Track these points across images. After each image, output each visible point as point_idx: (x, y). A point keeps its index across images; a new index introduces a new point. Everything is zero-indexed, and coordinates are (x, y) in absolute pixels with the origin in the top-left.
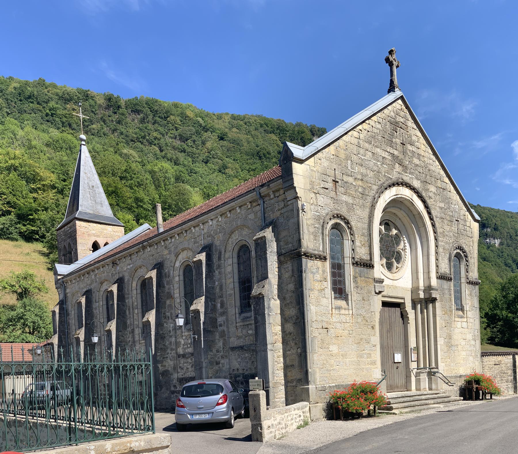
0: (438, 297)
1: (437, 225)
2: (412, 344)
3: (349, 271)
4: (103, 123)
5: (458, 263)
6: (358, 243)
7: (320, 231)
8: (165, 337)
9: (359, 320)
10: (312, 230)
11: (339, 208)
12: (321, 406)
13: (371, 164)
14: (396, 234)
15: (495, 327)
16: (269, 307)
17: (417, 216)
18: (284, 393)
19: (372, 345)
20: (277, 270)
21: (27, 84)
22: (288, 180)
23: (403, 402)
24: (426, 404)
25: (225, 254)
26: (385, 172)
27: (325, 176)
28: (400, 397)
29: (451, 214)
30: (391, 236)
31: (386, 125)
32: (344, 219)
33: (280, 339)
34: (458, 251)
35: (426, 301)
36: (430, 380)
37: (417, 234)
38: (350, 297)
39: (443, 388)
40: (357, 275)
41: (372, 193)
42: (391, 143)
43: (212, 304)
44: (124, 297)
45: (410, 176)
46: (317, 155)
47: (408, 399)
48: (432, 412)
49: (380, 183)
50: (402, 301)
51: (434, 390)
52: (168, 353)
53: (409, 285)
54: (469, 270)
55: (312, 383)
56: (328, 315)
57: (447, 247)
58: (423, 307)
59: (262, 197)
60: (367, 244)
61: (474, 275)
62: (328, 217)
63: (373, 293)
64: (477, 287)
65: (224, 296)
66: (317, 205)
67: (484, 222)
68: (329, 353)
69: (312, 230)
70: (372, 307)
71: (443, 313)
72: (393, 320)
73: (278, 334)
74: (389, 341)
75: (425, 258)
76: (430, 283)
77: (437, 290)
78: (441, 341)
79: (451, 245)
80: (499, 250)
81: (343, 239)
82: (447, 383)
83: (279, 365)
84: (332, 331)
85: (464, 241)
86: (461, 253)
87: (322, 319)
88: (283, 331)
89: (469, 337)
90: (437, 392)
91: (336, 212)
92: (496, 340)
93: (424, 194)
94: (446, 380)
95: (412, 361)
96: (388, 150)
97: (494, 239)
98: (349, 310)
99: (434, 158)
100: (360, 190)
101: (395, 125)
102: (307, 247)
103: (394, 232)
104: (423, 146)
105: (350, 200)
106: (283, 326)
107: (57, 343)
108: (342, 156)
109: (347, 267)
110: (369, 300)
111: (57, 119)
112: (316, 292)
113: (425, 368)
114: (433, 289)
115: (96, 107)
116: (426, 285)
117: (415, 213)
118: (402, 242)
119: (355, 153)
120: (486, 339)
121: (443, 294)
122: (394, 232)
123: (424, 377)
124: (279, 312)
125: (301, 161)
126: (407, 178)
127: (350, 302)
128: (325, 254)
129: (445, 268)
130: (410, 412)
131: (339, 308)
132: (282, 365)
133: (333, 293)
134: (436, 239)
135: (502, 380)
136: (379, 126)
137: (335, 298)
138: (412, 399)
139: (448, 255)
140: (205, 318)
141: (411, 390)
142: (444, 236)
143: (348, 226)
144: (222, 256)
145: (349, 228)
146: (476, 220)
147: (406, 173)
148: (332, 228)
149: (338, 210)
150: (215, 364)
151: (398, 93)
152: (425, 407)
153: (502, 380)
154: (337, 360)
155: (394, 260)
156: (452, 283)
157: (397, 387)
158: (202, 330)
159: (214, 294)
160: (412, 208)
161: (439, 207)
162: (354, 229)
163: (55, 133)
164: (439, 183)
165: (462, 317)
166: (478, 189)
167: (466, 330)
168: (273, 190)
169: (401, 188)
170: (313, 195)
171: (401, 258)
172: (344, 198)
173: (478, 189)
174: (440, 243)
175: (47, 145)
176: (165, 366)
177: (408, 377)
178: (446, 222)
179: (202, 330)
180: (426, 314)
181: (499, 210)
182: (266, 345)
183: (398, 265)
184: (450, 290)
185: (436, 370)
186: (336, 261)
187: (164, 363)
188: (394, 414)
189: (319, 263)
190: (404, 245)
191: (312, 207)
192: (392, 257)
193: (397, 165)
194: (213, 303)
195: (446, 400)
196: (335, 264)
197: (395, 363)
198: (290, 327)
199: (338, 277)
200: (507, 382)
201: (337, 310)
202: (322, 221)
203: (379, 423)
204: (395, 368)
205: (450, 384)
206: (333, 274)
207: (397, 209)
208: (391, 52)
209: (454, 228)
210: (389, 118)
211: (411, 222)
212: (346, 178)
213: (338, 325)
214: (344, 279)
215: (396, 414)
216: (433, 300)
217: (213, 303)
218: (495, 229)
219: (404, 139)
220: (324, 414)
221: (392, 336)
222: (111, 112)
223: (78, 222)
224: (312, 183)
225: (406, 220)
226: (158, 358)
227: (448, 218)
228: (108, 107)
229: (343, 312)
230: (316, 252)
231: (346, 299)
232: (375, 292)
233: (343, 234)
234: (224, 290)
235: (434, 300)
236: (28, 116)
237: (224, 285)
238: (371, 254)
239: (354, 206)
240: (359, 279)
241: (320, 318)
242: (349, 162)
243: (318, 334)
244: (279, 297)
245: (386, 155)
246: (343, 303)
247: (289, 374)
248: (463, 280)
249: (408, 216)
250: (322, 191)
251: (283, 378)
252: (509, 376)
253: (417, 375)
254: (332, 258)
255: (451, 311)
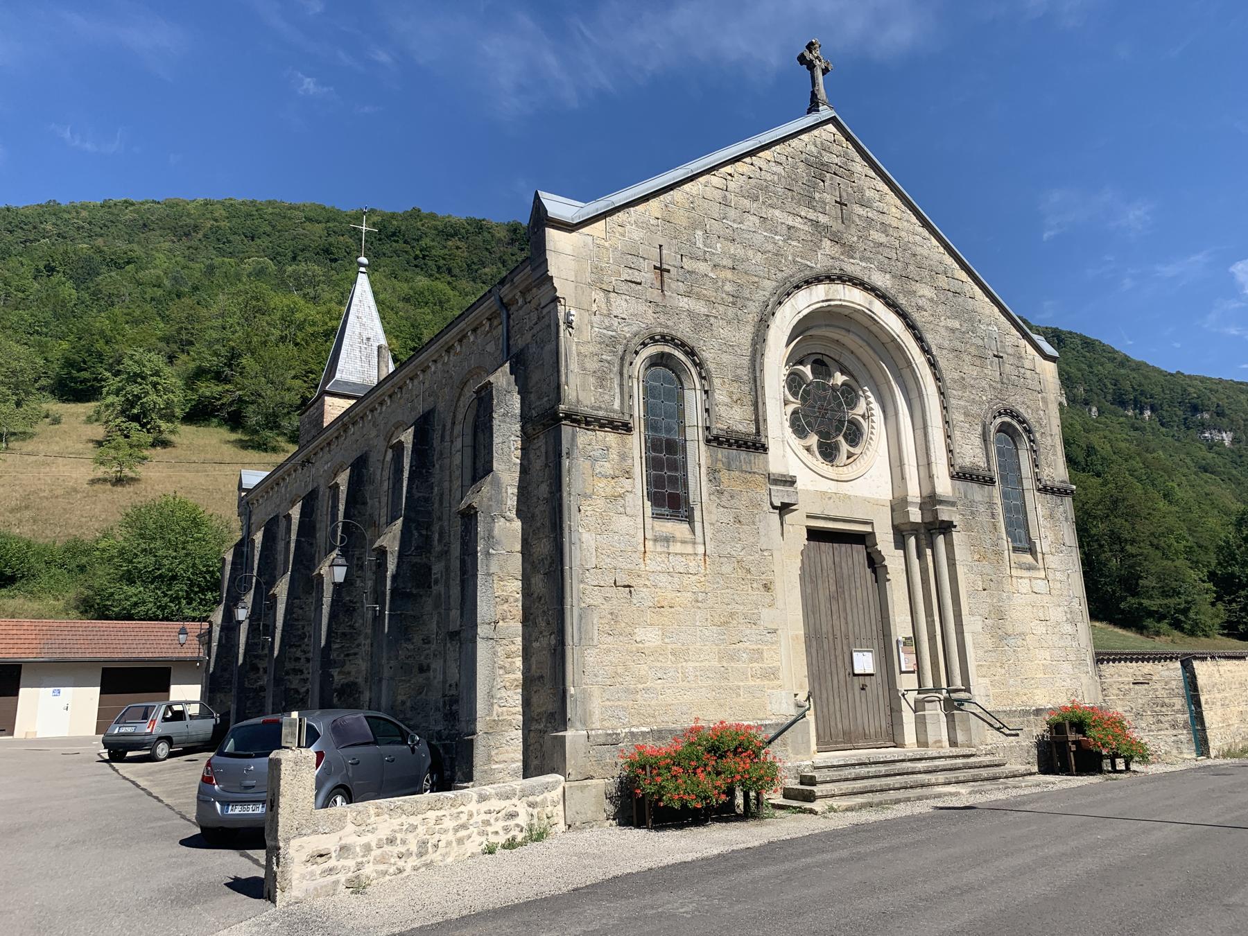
0: (956, 519)
1: (942, 363)
2: (901, 627)
3: (698, 456)
4: (500, 265)
5: (1013, 446)
6: (720, 396)
7: (616, 369)
8: (354, 610)
9: (726, 569)
10: (592, 365)
11: (670, 323)
12: (604, 783)
13: (758, 239)
14: (843, 384)
15: (1234, 600)
16: (490, 536)
17: (890, 346)
18: (521, 747)
19: (766, 628)
20: (519, 453)
21: (393, 216)
22: (540, 265)
23: (854, 779)
24: (923, 786)
25: (452, 429)
26: (794, 255)
27: (635, 259)
28: (853, 765)
29: (980, 342)
30: (834, 388)
31: (795, 167)
32: (665, 339)
33: (517, 610)
34: (1007, 419)
35: (927, 530)
36: (951, 719)
37: (897, 382)
38: (697, 514)
39: (987, 740)
40: (720, 465)
41: (761, 296)
42: (810, 202)
43: (421, 535)
44: (314, 527)
45: (864, 264)
46: (615, 217)
47: (883, 769)
48: (923, 808)
49: (780, 275)
50: (868, 529)
51: (962, 746)
52: (359, 645)
53: (885, 493)
54: (1042, 462)
55: (578, 725)
56: (634, 555)
57: (974, 409)
58: (924, 542)
59: (505, 305)
60: (748, 400)
61: (1057, 470)
62: (637, 340)
63: (767, 507)
64: (1068, 500)
65: (445, 517)
66: (609, 315)
67: (1194, 401)
68: (634, 647)
69: (592, 365)
70: (763, 539)
71: (976, 557)
72: (845, 571)
73: (511, 599)
74: (836, 622)
75: (920, 432)
76: (934, 488)
77: (953, 504)
78: (972, 626)
79: (986, 407)
80: (1233, 451)
81: (682, 388)
82: (998, 729)
83: (512, 676)
84: (643, 594)
85: (1020, 399)
86: (1014, 423)
87: (614, 563)
88: (527, 592)
89: (1057, 614)
90: (967, 751)
91: (659, 330)
92: (1241, 627)
93: (902, 301)
94: (993, 721)
95: (901, 672)
96: (803, 214)
97: (1219, 431)
98: (694, 543)
99: (926, 233)
100: (728, 287)
101: (819, 169)
102: (578, 401)
103: (839, 379)
104: (894, 210)
105: (701, 308)
106: (526, 579)
107: (219, 621)
108: (681, 218)
109: (691, 448)
110: (754, 523)
111: (430, 263)
112: (601, 503)
113: (937, 689)
114: (941, 502)
115: (493, 244)
116: (924, 494)
117: (886, 339)
118: (862, 401)
119: (716, 216)
120: (1216, 626)
121: (972, 513)
122: (839, 379)
123: (935, 712)
124: (518, 547)
125: (569, 227)
126: (853, 267)
127: (698, 525)
128: (627, 418)
129: (972, 453)
130: (862, 807)
131: (667, 540)
132: (519, 675)
133: (648, 504)
134: (942, 394)
135: (1159, 721)
136: (779, 169)
137: (657, 516)
138: (883, 769)
139: (980, 429)
140: (398, 566)
141: (902, 746)
142: (964, 387)
143: (694, 361)
144: (448, 433)
145: (695, 364)
146: (1046, 357)
147: (852, 257)
148: (652, 365)
149: (667, 327)
150: (415, 670)
151: (825, 112)
152: (919, 791)
153: (1159, 721)
154: (659, 664)
155: (841, 438)
156: (996, 491)
157: (865, 736)
158: (388, 592)
159: (430, 513)
160: (874, 328)
161: (947, 328)
162: (711, 366)
163: (422, 281)
164: (942, 281)
165: (1030, 568)
166: (1178, 345)
167: (1047, 598)
168: (522, 287)
169: (839, 287)
170: (599, 296)
171: (862, 435)
172: (684, 303)
173: (1178, 345)
174: (953, 401)
175: (407, 300)
176: (349, 673)
177: (895, 712)
178: (967, 358)
179: (388, 592)
180: (930, 559)
181: (1221, 380)
182: (475, 626)
183: (851, 449)
184: (991, 505)
185: (963, 695)
186: (664, 435)
187: (347, 668)
188: (812, 811)
189: (611, 438)
190: (867, 406)
191: (596, 319)
192: (830, 428)
193: (827, 243)
194: (424, 532)
195: (991, 773)
196: (660, 440)
197: (855, 675)
198: (538, 581)
199: (669, 470)
200: (1173, 727)
201: (658, 544)
202: (620, 348)
203: (716, 843)
204: (857, 688)
205: (1008, 732)
206: (653, 464)
207: (838, 331)
208: (810, 47)
209: (992, 371)
210: (804, 156)
211: (877, 358)
212: (688, 264)
213: (664, 579)
214: (686, 475)
215: (816, 813)
216: (947, 528)
217: (424, 532)
218: (1218, 415)
219: (844, 194)
220: (611, 809)
221: (845, 610)
222: (515, 249)
223: (328, 399)
224: (597, 270)
225: (865, 353)
226: (333, 656)
227: (973, 350)
228: (512, 242)
229: (677, 548)
230: (601, 413)
231: (690, 520)
232: (771, 504)
233: (683, 378)
234: (446, 504)
235: (947, 528)
236: (388, 261)
237: (446, 492)
238: (759, 420)
239: (712, 320)
240: (724, 475)
241: (608, 560)
242: (699, 233)
243: (601, 600)
244: (519, 514)
245: (797, 223)
246: (680, 529)
247: (534, 700)
248: (1028, 484)
249: (869, 345)
250: (624, 287)
251: (520, 709)
252: (1178, 712)
253: (919, 706)
254: (651, 426)
255: (999, 553)
